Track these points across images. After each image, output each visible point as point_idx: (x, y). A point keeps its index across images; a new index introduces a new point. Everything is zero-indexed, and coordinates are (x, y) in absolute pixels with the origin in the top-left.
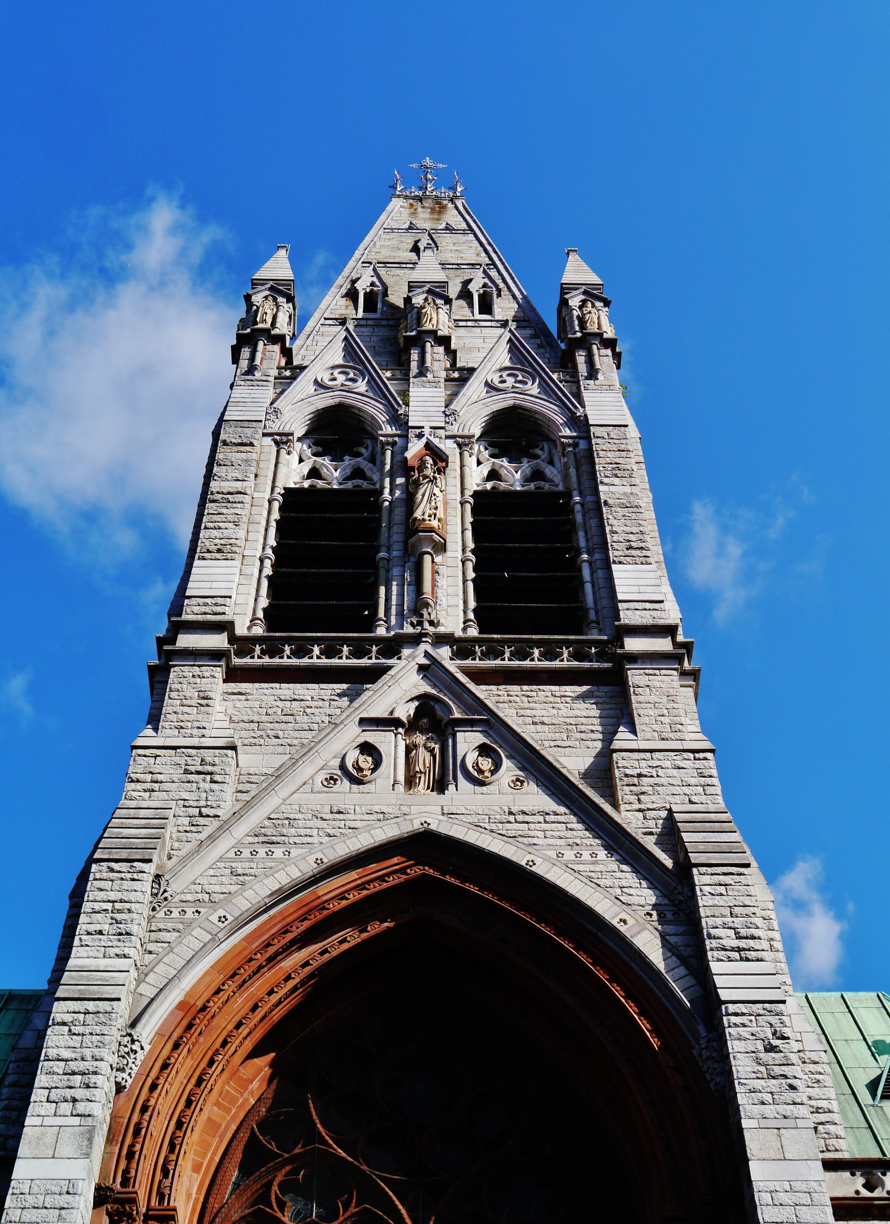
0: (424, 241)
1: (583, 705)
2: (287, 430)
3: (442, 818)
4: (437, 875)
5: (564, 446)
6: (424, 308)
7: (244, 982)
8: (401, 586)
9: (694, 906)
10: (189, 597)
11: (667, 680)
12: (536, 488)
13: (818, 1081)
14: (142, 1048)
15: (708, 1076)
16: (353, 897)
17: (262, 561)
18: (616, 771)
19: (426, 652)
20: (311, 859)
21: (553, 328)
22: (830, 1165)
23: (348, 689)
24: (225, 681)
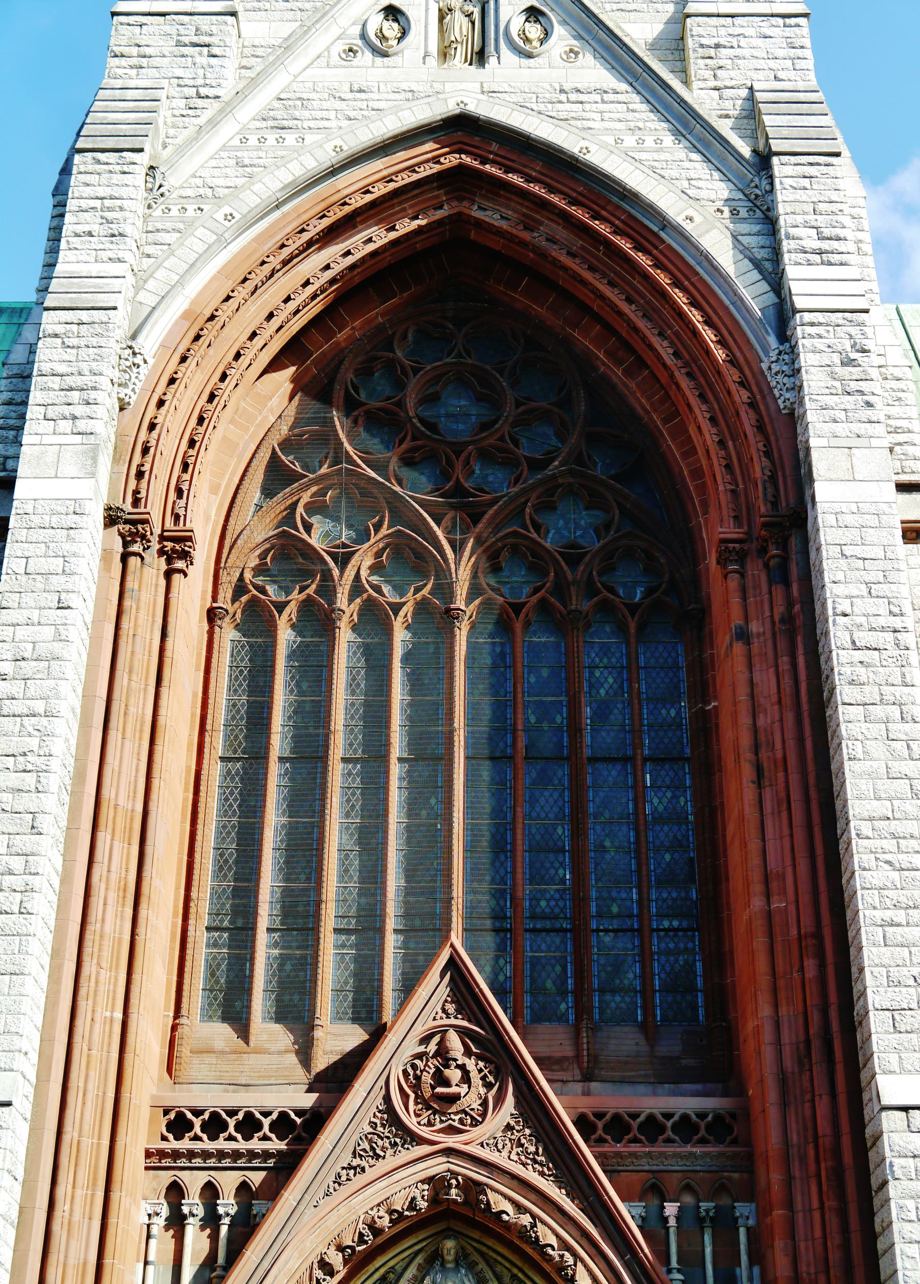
13: (899, 399)
14: (145, 362)
15: (776, 392)
16: (380, 190)
20: (329, 147)
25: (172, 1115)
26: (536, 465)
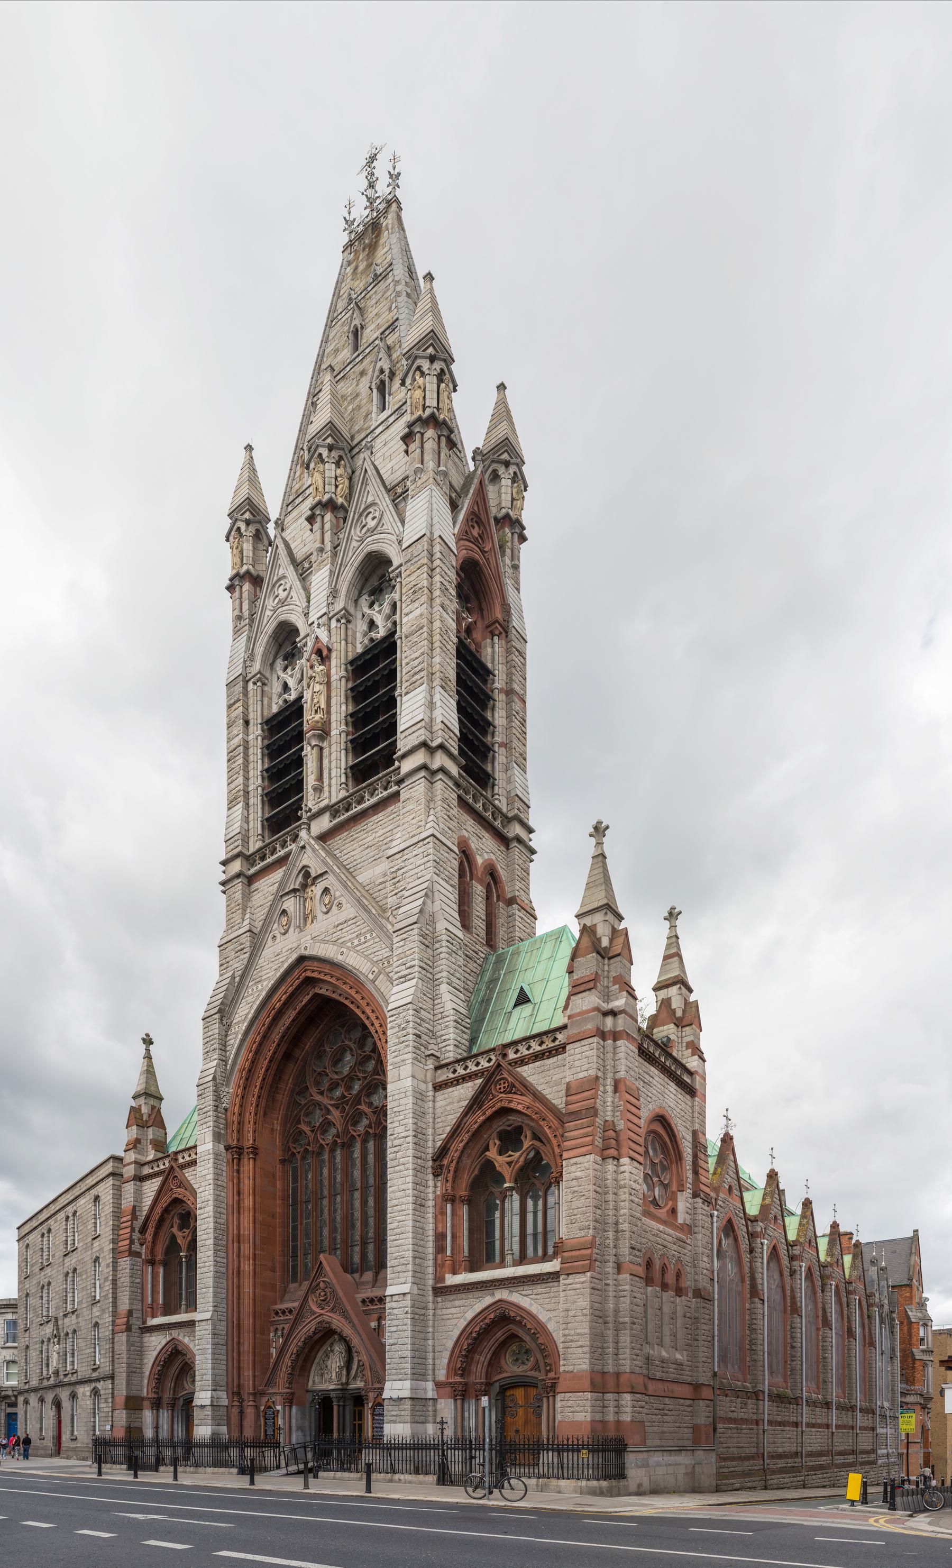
0: (180, 1451)
1: (512, 1314)
2: (191, 1144)
4: (339, 1171)
5: (583, 1448)
6: (78, 1323)
7: (475, 689)
8: (333, 1220)
9: (588, 1081)
10: (601, 884)
11: (503, 750)
12: (493, 1294)
17: (853, 1452)
18: (478, 857)
19: (293, 711)
21: (479, 1082)
22: (807, 1204)
23: (158, 1304)
24: (670, 999)
26: (365, 1078)
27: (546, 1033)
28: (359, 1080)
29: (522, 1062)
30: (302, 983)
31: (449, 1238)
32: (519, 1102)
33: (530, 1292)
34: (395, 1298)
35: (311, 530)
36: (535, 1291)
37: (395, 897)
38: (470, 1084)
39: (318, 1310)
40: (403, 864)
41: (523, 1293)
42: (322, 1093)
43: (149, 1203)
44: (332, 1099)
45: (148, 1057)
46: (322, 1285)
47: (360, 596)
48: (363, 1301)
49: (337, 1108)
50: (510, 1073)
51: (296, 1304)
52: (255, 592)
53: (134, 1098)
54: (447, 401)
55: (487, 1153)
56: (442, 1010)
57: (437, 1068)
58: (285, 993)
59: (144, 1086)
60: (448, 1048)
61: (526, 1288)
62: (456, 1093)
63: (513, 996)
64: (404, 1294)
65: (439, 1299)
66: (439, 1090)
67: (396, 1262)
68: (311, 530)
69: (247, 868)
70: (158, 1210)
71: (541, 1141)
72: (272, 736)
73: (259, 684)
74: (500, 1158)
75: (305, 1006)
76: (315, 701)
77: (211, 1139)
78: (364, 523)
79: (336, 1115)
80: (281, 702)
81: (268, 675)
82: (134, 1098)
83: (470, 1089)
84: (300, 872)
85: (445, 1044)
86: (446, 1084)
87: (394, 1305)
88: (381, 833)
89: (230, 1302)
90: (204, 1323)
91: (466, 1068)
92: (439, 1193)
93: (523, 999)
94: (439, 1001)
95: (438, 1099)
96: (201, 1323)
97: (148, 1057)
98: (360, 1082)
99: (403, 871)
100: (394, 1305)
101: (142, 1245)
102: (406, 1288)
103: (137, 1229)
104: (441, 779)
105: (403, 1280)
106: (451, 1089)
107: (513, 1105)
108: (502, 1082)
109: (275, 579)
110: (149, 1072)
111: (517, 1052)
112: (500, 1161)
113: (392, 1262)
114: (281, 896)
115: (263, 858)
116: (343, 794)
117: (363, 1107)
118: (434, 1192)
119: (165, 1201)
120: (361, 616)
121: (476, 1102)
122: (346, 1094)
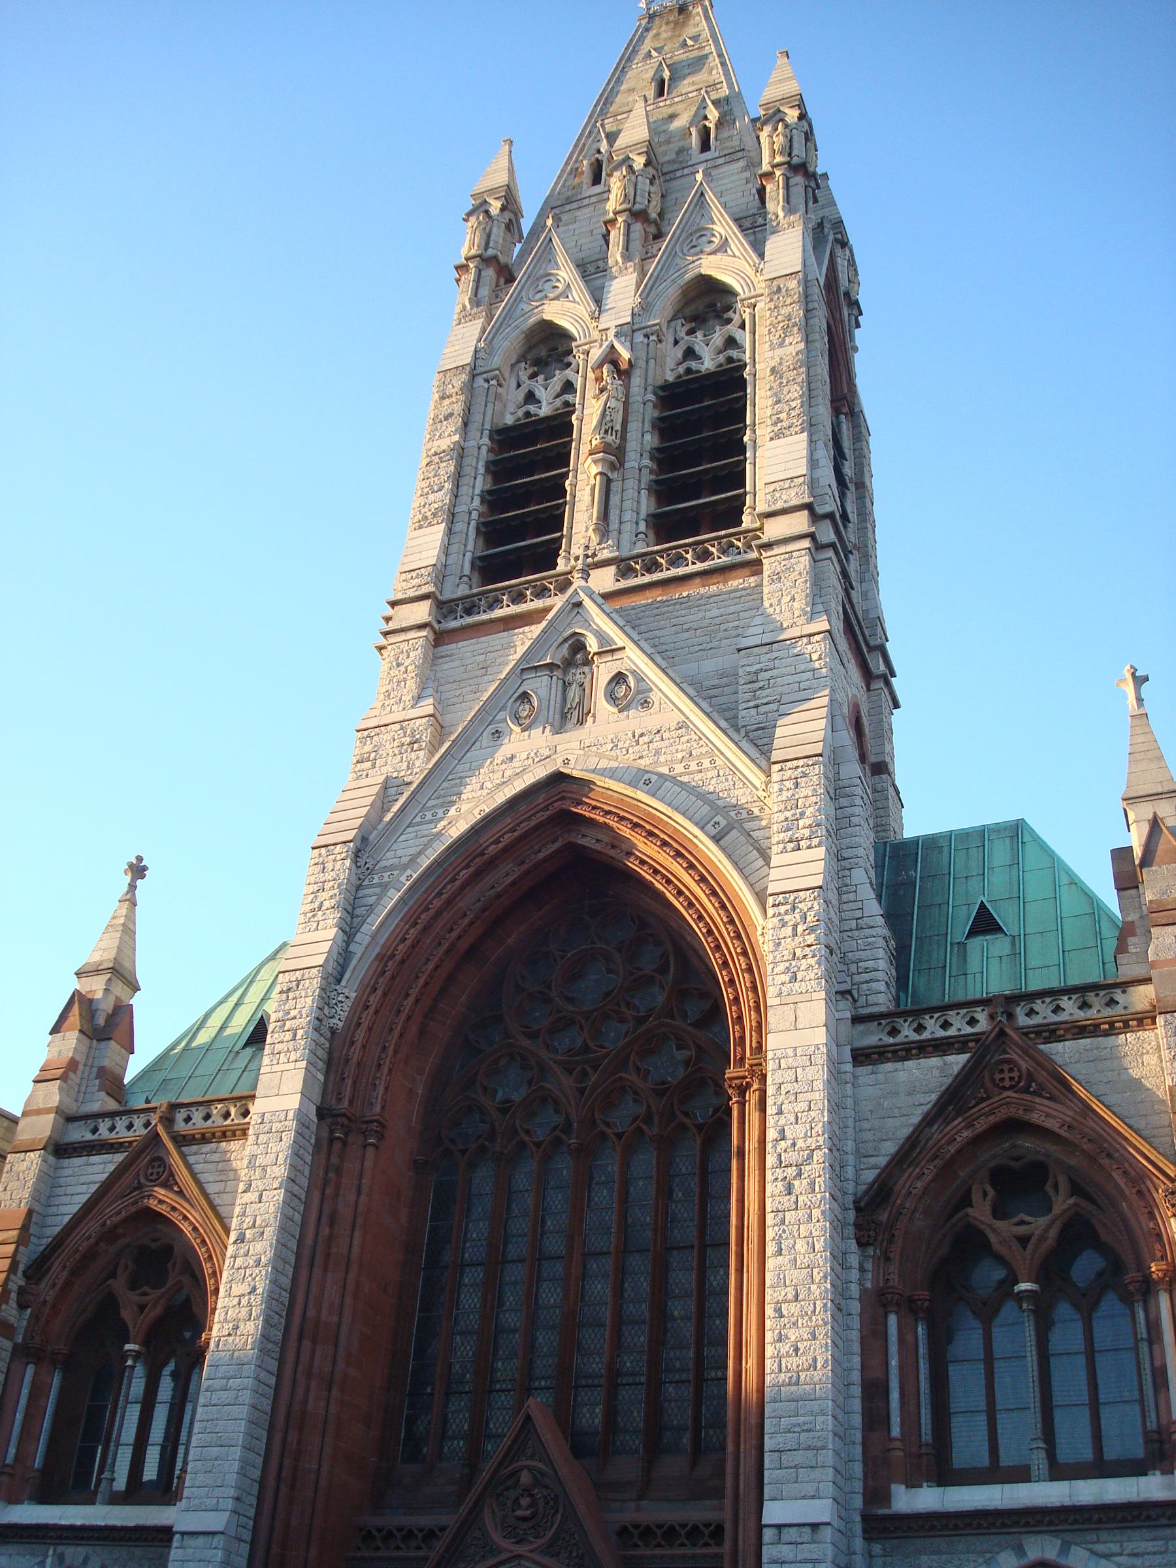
3: (581, 752)
20: (476, 812)
21: (958, 1061)
25: (364, 1533)
26: (640, 1021)
27: (1095, 987)
28: (622, 1021)
29: (1052, 1033)
30: (551, 820)
31: (895, 1396)
32: (1045, 1114)
33: (1115, 1548)
34: (791, 1534)
35: (458, 281)
36: (1130, 1547)
37: (753, 712)
38: (934, 1061)
39: (506, 1544)
40: (771, 665)
41: (1100, 1548)
42: (533, 1035)
43: (75, 1209)
44: (555, 1050)
45: (130, 899)
46: (525, 1478)
47: (518, 362)
48: (623, 1532)
49: (570, 1071)
50: (1025, 1051)
51: (449, 1520)
52: (498, 281)
53: (79, 974)
54: (1169, 1513)
55: (970, 1210)
56: (858, 914)
57: (856, 1020)
58: (512, 830)
59: (112, 954)
60: (874, 985)
61: (1104, 1535)
62: (902, 1076)
63: (963, 919)
64: (815, 1526)
65: (877, 1548)
66: (862, 1064)
67: (790, 1440)
68: (458, 281)
69: (452, 618)
70: (91, 1228)
71: (1093, 1201)
72: (501, 452)
73: (494, 382)
74: (999, 1224)
75: (545, 860)
76: (608, 418)
77: (299, 1087)
78: (540, 288)
79: (563, 1084)
80: (520, 413)
81: (507, 375)
82: (79, 974)
83: (936, 1073)
84: (566, 640)
85: (866, 977)
86: (881, 1054)
87: (786, 1551)
88: (715, 612)
89: (270, 1493)
90: (201, 1540)
91: (920, 1028)
92: (869, 1285)
93: (985, 924)
94: (852, 896)
95: (861, 1080)
96: (189, 1541)
97: (130, 899)
98: (624, 1028)
99: (770, 674)
100: (786, 1551)
101: (22, 1306)
102: (821, 1510)
103: (21, 1267)
104: (830, 559)
105: (810, 1489)
106: (889, 1066)
107: (1036, 1118)
108: (1006, 1067)
109: (541, 272)
110: (128, 931)
111: (1031, 1013)
112: (1000, 1232)
113: (780, 1438)
114: (523, 670)
115: (469, 612)
116: (463, 590)
117: (631, 1077)
118: (861, 1282)
119: (114, 1212)
120: (515, 385)
121: (953, 1101)
122: (591, 1044)
